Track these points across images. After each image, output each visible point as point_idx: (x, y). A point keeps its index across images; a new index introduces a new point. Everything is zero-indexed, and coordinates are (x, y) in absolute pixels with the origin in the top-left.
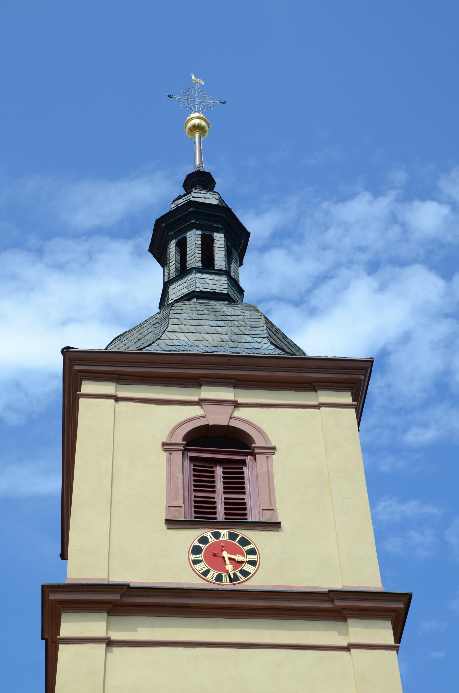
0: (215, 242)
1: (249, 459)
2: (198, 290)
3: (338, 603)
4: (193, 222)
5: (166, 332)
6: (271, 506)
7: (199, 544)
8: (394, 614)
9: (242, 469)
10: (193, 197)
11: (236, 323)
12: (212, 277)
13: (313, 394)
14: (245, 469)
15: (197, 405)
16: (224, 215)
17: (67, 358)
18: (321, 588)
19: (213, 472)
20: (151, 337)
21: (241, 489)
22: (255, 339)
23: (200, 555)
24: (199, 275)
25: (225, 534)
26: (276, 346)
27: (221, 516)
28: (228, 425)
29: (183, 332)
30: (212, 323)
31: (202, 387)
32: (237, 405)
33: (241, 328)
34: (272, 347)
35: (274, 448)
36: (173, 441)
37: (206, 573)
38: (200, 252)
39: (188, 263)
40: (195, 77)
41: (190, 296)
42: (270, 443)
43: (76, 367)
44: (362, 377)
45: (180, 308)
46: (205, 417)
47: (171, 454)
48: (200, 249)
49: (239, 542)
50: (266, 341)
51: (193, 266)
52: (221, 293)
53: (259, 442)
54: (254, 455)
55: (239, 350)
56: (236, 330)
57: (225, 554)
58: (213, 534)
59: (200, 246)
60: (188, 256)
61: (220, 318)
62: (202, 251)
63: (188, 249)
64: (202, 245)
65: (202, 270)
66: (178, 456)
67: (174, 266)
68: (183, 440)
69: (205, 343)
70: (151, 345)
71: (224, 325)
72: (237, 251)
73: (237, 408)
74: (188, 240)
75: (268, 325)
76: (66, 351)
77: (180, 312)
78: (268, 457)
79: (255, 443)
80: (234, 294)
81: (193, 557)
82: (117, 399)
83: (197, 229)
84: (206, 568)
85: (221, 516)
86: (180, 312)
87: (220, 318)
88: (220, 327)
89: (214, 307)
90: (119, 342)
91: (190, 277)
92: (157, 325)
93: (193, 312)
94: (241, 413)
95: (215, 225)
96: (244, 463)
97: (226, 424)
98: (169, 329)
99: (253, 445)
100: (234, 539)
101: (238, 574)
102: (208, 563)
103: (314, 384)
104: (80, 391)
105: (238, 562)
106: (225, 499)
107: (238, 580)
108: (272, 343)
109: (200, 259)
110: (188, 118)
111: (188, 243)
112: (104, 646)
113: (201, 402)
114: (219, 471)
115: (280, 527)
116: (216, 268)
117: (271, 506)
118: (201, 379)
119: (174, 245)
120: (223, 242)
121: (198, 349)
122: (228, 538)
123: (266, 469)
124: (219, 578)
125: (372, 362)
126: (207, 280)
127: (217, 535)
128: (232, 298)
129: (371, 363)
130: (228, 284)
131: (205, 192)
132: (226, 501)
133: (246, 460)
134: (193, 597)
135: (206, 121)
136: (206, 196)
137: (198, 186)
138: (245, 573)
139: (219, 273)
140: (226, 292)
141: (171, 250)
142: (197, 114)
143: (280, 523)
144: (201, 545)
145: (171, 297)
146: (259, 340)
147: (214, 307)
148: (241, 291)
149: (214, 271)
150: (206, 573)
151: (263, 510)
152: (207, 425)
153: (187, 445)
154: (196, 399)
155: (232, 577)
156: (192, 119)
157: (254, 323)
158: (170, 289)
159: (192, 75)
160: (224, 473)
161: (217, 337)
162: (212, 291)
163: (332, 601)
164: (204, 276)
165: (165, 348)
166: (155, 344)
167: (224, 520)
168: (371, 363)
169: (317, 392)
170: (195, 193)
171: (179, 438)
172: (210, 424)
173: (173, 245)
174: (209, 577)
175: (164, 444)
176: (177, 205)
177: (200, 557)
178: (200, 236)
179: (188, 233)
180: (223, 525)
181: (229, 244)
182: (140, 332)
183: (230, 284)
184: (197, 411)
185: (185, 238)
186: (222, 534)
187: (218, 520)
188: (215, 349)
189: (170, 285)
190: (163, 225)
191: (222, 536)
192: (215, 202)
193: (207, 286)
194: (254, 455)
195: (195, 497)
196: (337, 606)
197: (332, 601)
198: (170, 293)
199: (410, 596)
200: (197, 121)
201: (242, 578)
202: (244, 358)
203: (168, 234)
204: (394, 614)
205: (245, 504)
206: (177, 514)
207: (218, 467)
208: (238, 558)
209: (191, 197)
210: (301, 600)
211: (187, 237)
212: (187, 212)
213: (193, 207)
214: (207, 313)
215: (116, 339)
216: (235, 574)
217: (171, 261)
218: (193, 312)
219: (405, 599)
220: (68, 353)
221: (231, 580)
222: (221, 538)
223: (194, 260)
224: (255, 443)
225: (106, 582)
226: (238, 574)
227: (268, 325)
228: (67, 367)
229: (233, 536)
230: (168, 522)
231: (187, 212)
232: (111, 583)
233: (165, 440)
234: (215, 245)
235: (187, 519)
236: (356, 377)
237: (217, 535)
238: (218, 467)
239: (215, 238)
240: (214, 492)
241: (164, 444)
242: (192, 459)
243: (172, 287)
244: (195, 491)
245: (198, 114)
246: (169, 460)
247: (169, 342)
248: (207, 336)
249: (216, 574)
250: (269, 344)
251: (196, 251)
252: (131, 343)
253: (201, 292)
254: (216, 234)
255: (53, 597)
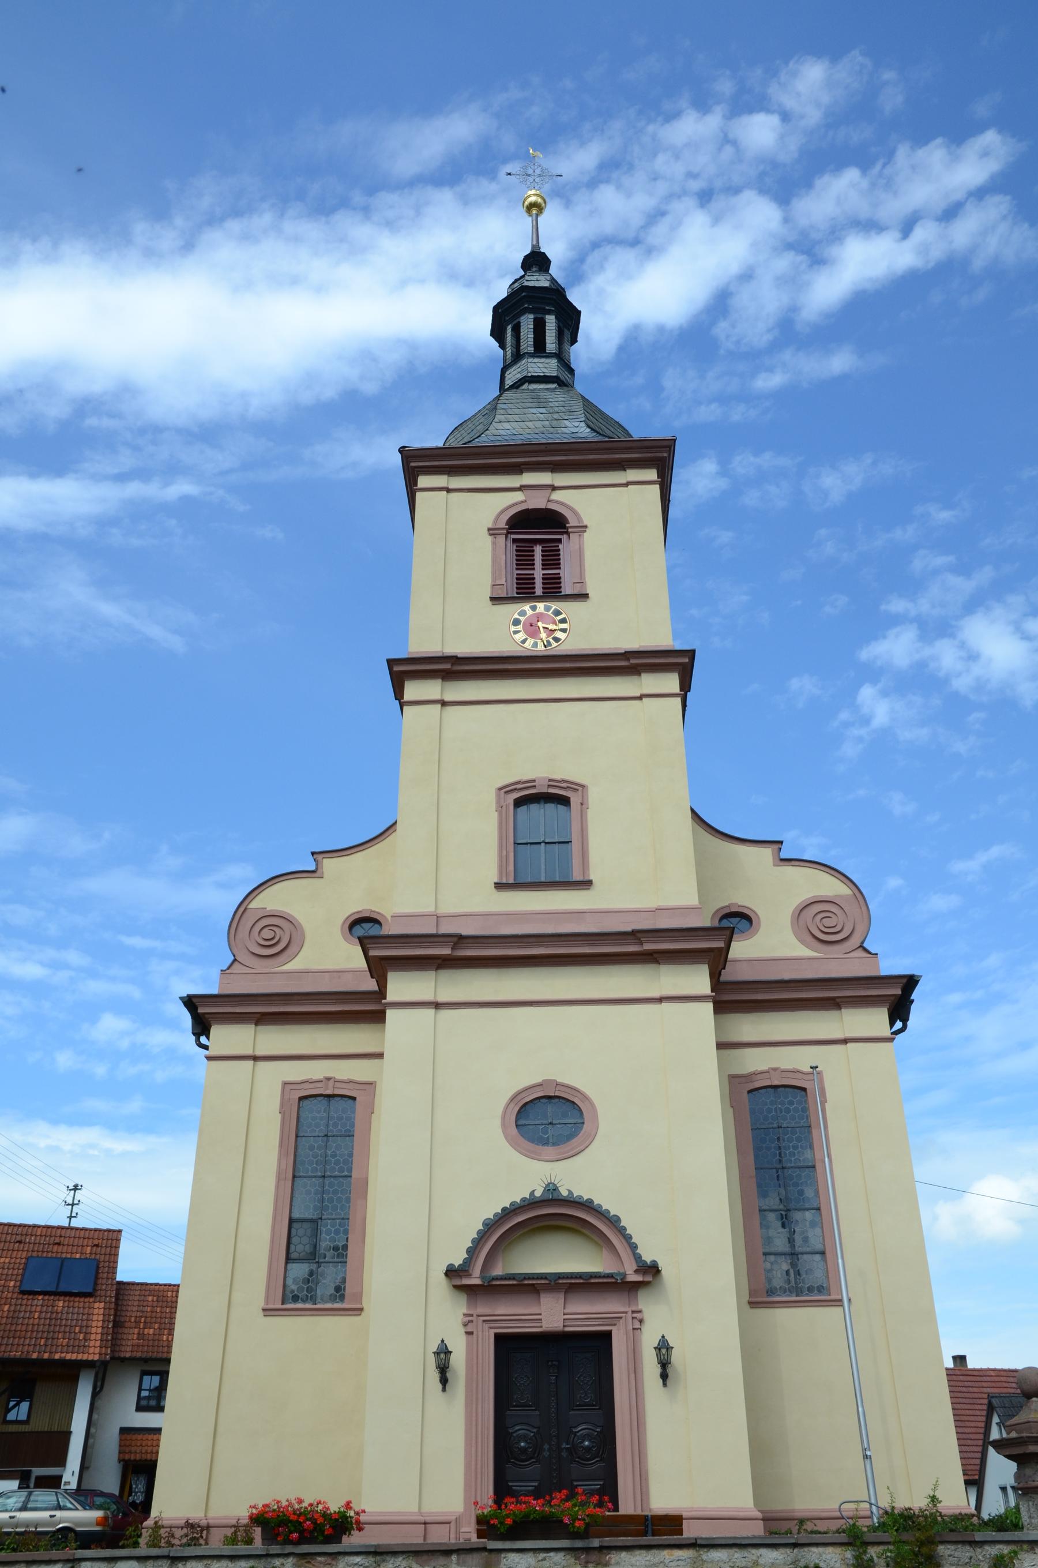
0: (547, 324)
1: (564, 537)
2: (529, 375)
3: (633, 661)
4: (526, 307)
5: (493, 423)
6: (581, 579)
7: (518, 617)
8: (681, 667)
9: (558, 546)
10: (527, 281)
11: (556, 409)
12: (543, 360)
13: (622, 473)
14: (561, 547)
15: (519, 491)
16: (554, 297)
17: (404, 455)
18: (621, 648)
19: (533, 551)
20: (480, 428)
21: (557, 565)
22: (573, 423)
23: (519, 626)
24: (530, 360)
25: (541, 606)
26: (592, 429)
27: (539, 591)
28: (546, 509)
29: (509, 422)
30: (534, 411)
31: (524, 474)
32: (554, 488)
33: (560, 414)
34: (588, 430)
35: (586, 527)
36: (497, 527)
37: (524, 642)
38: (533, 336)
39: (521, 348)
40: (533, 151)
41: (523, 380)
42: (583, 523)
43: (412, 464)
44: (665, 455)
45: (507, 398)
46: (525, 501)
47: (495, 537)
48: (532, 333)
49: (553, 613)
50: (583, 424)
51: (526, 351)
52: (550, 376)
53: (572, 522)
54: (568, 533)
55: (558, 436)
56: (556, 416)
57: (540, 624)
58: (530, 607)
59: (532, 330)
60: (521, 341)
61: (542, 404)
62: (534, 335)
63: (522, 334)
64: (534, 329)
65: (533, 355)
66: (501, 539)
67: (510, 351)
68: (506, 525)
69: (528, 431)
70: (479, 436)
71: (546, 412)
72: (569, 330)
73: (554, 491)
74: (521, 325)
75: (586, 408)
76: (402, 450)
77: (506, 402)
78: (580, 535)
79: (569, 523)
80: (565, 376)
81: (513, 628)
82: (449, 490)
83: (530, 313)
84: (524, 637)
85: (539, 591)
86: (506, 402)
87: (542, 404)
88: (542, 414)
89: (538, 394)
90: (458, 432)
91: (524, 362)
92: (486, 416)
93: (518, 401)
94: (557, 496)
95: (547, 308)
96: (560, 541)
97: (543, 507)
98: (496, 420)
99: (567, 525)
100: (548, 611)
101: (551, 640)
102: (526, 632)
103: (623, 463)
104: (417, 486)
105: (551, 630)
106: (543, 574)
107: (551, 645)
108: (588, 426)
109: (532, 343)
110: (526, 196)
111: (521, 328)
112: (440, 706)
113: (521, 488)
114: (538, 550)
115: (588, 597)
116: (547, 351)
117: (581, 579)
118: (523, 466)
119: (510, 330)
120: (554, 324)
121: (521, 437)
122: (543, 610)
123: (578, 546)
124: (535, 645)
125: (675, 440)
126: (538, 364)
127: (534, 608)
128: (563, 382)
129: (673, 441)
130: (558, 366)
131: (538, 274)
132: (544, 576)
133: (561, 539)
134: (510, 663)
135: (542, 198)
136: (540, 278)
137: (534, 266)
138: (556, 640)
139: (550, 356)
140: (555, 374)
141: (508, 335)
142: (533, 192)
143: (588, 594)
144: (520, 618)
145: (507, 383)
146: (576, 424)
147: (538, 394)
148: (571, 371)
149: (544, 355)
150: (524, 642)
151: (574, 583)
152: (528, 510)
153: (510, 528)
154: (517, 485)
155: (546, 644)
156: (529, 196)
157: (572, 408)
158: (506, 375)
159: (530, 148)
160: (542, 551)
161: (539, 424)
162: (542, 374)
163: (628, 660)
164: (536, 360)
165: (492, 438)
166: (483, 435)
167: (542, 594)
168: (673, 441)
169: (626, 471)
170: (529, 276)
171: (502, 524)
172: (530, 508)
173: (509, 329)
174: (526, 645)
175: (489, 529)
176: (513, 290)
177: (519, 628)
178: (533, 320)
179: (522, 318)
180: (539, 599)
181: (561, 325)
182: (473, 423)
183: (559, 365)
184: (519, 496)
185: (519, 323)
186: (538, 607)
187: (536, 594)
188: (536, 436)
189: (506, 371)
190: (500, 311)
191: (538, 608)
192: (547, 284)
193: (538, 370)
194: (568, 533)
195: (517, 574)
196: (632, 663)
197: (628, 660)
198: (506, 379)
199: (693, 652)
200: (533, 199)
201: (554, 644)
202: (559, 445)
203: (505, 319)
204: (681, 667)
205: (560, 578)
206: (500, 592)
207: (538, 546)
208: (552, 627)
209: (524, 281)
210: (602, 660)
211: (521, 321)
212: (520, 297)
213: (525, 292)
214: (531, 400)
215: (456, 428)
216: (548, 642)
217: (507, 347)
218: (518, 401)
219: (690, 654)
220: (404, 452)
221: (545, 646)
222: (537, 610)
223: (526, 345)
224: (569, 523)
225: (440, 655)
226: (551, 640)
227: (586, 408)
228: (405, 462)
229: (547, 609)
230: (492, 599)
231: (520, 297)
232: (445, 655)
233: (490, 526)
234: (547, 328)
235: (510, 596)
236: (660, 455)
237: (534, 608)
238: (538, 546)
239: (547, 321)
240: (534, 569)
241: (489, 529)
242: (515, 541)
243: (508, 372)
244: (517, 569)
245: (534, 191)
246: (494, 543)
247: (496, 432)
248: (530, 424)
249: (532, 642)
250: (585, 427)
251: (529, 336)
252: (466, 434)
253: (532, 376)
254: (547, 317)
255: (396, 668)
